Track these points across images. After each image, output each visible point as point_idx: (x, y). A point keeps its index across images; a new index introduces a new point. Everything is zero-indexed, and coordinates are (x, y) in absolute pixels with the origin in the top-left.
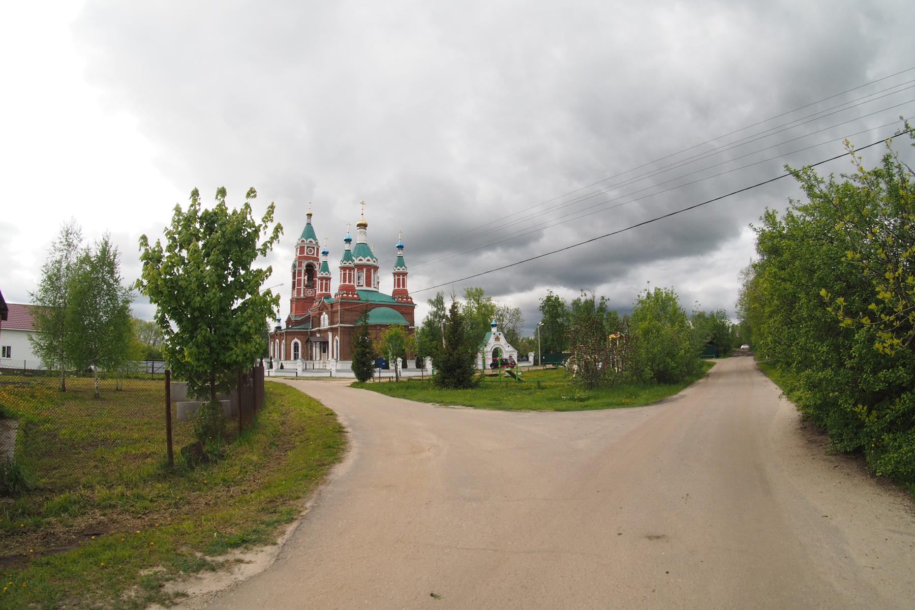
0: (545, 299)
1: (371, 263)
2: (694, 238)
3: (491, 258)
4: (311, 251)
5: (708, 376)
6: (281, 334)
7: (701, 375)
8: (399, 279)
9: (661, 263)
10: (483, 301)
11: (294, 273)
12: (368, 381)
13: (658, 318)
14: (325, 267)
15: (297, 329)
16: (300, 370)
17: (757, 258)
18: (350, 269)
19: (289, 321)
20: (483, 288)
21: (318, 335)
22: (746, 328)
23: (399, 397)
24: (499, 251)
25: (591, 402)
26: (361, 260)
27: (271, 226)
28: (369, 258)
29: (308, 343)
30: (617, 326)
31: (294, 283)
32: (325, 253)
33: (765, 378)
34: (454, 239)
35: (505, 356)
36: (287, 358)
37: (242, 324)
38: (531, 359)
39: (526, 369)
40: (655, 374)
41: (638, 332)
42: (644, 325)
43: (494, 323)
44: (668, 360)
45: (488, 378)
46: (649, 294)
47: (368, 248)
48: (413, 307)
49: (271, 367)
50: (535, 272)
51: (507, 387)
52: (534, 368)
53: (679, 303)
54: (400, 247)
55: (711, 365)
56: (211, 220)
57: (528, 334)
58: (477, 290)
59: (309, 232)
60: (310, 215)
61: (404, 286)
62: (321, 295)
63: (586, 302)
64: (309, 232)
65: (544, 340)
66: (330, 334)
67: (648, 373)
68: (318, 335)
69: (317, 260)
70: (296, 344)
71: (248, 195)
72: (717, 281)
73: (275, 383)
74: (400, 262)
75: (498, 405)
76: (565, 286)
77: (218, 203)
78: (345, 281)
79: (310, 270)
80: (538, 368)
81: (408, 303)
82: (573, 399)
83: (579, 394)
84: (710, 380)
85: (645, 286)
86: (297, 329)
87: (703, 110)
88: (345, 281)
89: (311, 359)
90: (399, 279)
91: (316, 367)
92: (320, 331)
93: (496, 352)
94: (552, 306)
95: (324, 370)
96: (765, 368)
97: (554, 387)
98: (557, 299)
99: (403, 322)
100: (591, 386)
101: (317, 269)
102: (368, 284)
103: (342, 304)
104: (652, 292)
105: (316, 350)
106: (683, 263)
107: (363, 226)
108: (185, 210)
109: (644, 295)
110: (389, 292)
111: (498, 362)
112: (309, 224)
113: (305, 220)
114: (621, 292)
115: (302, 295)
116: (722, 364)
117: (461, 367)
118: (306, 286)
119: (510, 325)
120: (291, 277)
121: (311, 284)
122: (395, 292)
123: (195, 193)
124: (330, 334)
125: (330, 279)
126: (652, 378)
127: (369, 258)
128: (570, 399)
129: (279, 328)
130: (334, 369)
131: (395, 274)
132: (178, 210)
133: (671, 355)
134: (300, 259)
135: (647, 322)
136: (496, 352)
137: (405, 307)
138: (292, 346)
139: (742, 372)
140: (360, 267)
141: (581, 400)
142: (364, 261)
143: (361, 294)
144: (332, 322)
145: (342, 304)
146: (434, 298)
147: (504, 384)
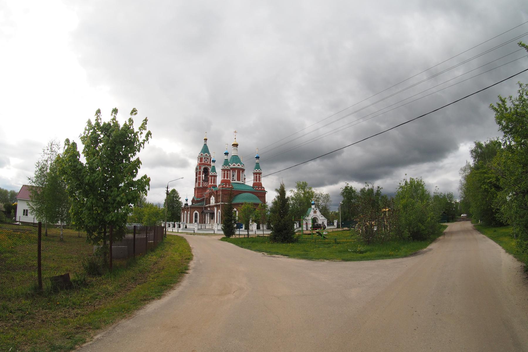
0: (344, 188)
1: (240, 167)
2: (433, 151)
3: (313, 165)
4: (206, 160)
5: (444, 234)
6: (188, 208)
7: (441, 234)
9: (413, 166)
10: (307, 190)
11: (197, 173)
12: (231, 237)
13: (412, 197)
14: (214, 169)
15: (197, 205)
16: (196, 229)
17: (471, 162)
18: (228, 170)
19: (193, 201)
20: (307, 182)
21: (209, 209)
22: (466, 203)
23: (245, 247)
24: (318, 161)
25: (368, 254)
26: (234, 165)
27: (145, 132)
28: (239, 164)
29: (203, 214)
30: (387, 204)
31: (196, 179)
32: (214, 161)
33: (481, 236)
34: (290, 154)
35: (320, 222)
36: (191, 222)
37: (118, 195)
38: (335, 224)
39: (331, 230)
40: (411, 234)
41: (400, 206)
42: (404, 201)
43: (313, 202)
44: (420, 224)
45: (306, 236)
46: (406, 182)
47: (239, 158)
48: (265, 193)
49: (180, 227)
50: (339, 173)
51: (315, 242)
52: (336, 230)
53: (426, 188)
54: (258, 158)
55: (446, 227)
56: (106, 128)
57: (334, 209)
58: (303, 183)
59: (205, 149)
60: (206, 140)
61: (259, 180)
62: (211, 185)
63: (369, 190)
64: (205, 149)
65: (344, 213)
66: (216, 209)
67: (406, 233)
68: (209, 209)
69: (210, 165)
70: (196, 214)
71: (132, 112)
72: (447, 176)
73: (180, 237)
74: (258, 166)
75: (305, 256)
76: (356, 181)
77: (112, 117)
78: (224, 177)
79: (206, 171)
80: (339, 230)
81: (262, 190)
82: (355, 252)
83: (361, 248)
84: (446, 237)
85: (403, 177)
86: (197, 205)
87: (434, 75)
88: (224, 177)
89: (205, 223)
90: (256, 177)
91: (207, 227)
92: (210, 207)
93: (314, 220)
94: (348, 193)
95: (212, 229)
96: (480, 229)
97: (345, 243)
98: (351, 188)
99: (258, 201)
100: (368, 243)
101: (210, 171)
102: (239, 179)
103: (222, 191)
104: (408, 181)
105: (208, 218)
106: (425, 166)
107: (236, 145)
108: (93, 123)
109: (403, 184)
111: (316, 226)
112: (205, 145)
113: (203, 142)
114: (389, 184)
115: (201, 186)
116: (451, 226)
117: (286, 229)
118: (204, 181)
119: (323, 204)
121: (206, 180)
122: (254, 184)
123: (99, 112)
124: (216, 209)
125: (216, 176)
126: (409, 237)
127: (239, 164)
128: (353, 252)
129: (186, 204)
130: (216, 229)
131: (254, 173)
132: (89, 123)
133: (422, 221)
134: (200, 165)
135: (405, 200)
136: (314, 220)
137: (260, 193)
138: (194, 215)
139: (466, 231)
140: (234, 169)
141: (361, 252)
142: (236, 166)
143: (234, 185)
144: (216, 201)
145: (222, 191)
146: (279, 188)
147: (314, 241)
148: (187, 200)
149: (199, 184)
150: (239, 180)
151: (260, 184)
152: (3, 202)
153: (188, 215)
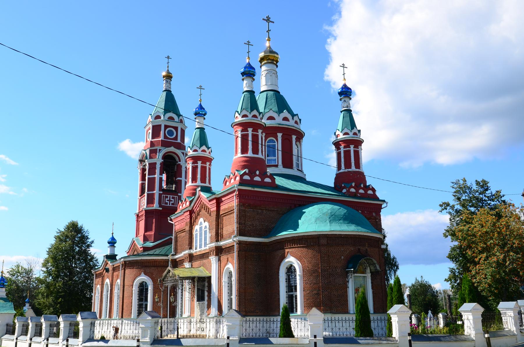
8: (347, 154)
70: (291, 270)
78: (244, 150)
81: (365, 196)
89: (173, 314)
90: (347, 154)
102: (288, 162)
105: (186, 297)
110: (329, 179)
120: (139, 177)
122: (339, 178)
125: (210, 160)
129: (112, 257)
138: (135, 290)
140: (271, 132)
148: (112, 243)
149: (150, 200)
150: (290, 166)
151: (360, 178)
152: (3, 286)
153: (117, 292)
